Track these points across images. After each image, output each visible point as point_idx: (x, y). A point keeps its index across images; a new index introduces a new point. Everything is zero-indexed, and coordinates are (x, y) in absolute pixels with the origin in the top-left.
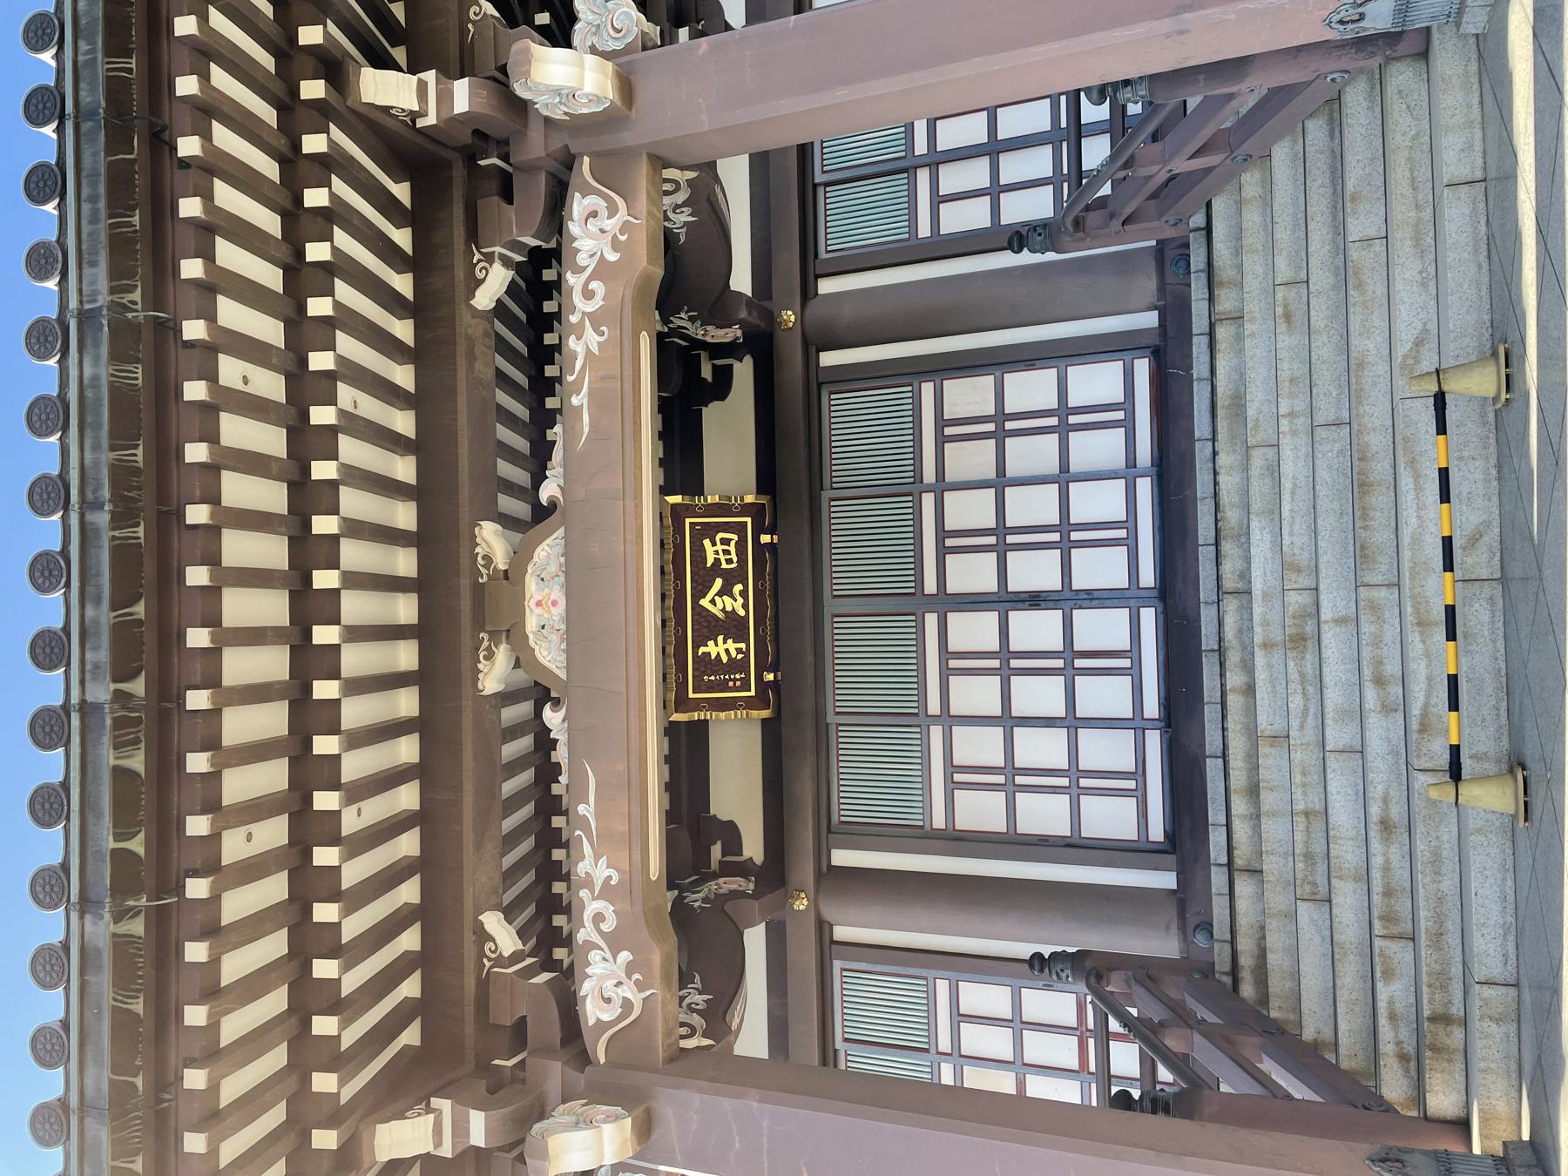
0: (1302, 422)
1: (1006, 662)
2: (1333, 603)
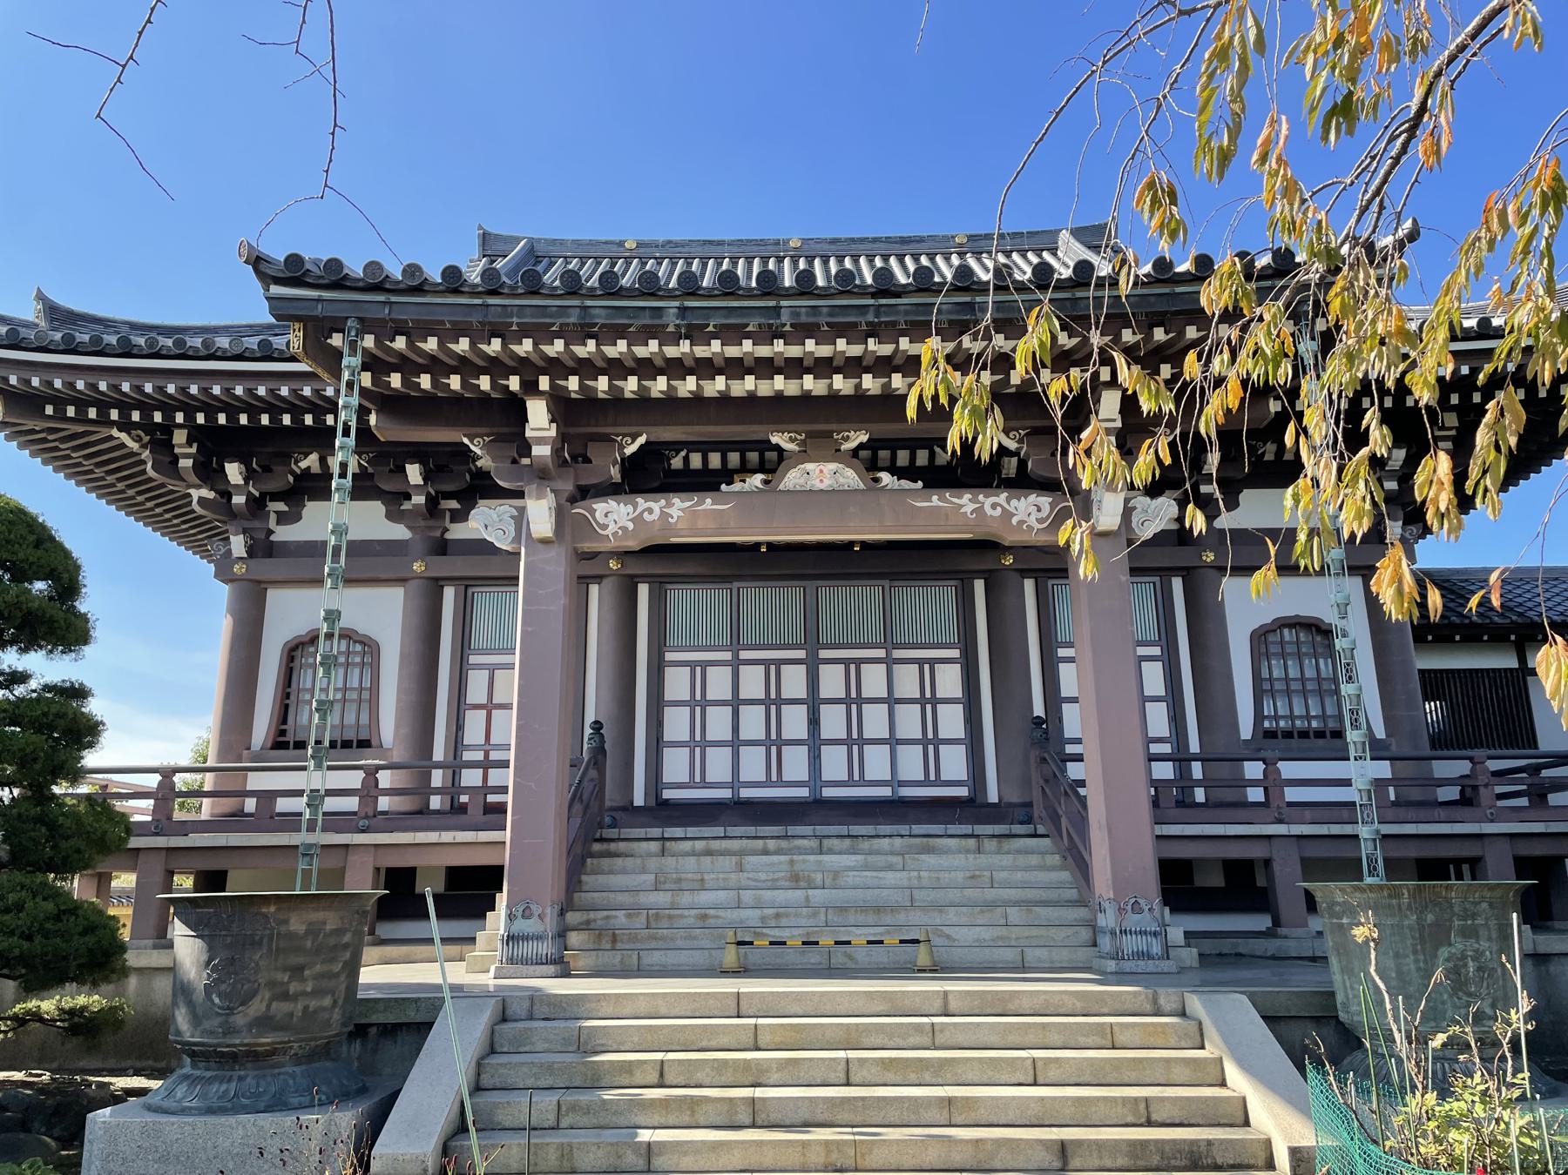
0: (915, 883)
1: (774, 702)
2: (817, 896)
